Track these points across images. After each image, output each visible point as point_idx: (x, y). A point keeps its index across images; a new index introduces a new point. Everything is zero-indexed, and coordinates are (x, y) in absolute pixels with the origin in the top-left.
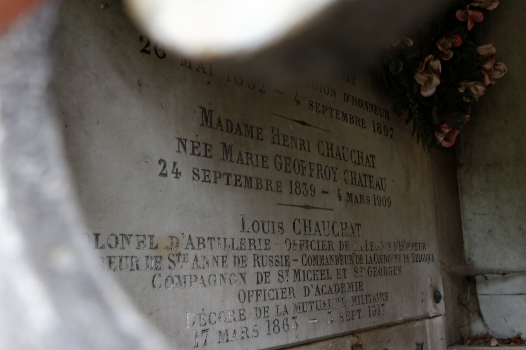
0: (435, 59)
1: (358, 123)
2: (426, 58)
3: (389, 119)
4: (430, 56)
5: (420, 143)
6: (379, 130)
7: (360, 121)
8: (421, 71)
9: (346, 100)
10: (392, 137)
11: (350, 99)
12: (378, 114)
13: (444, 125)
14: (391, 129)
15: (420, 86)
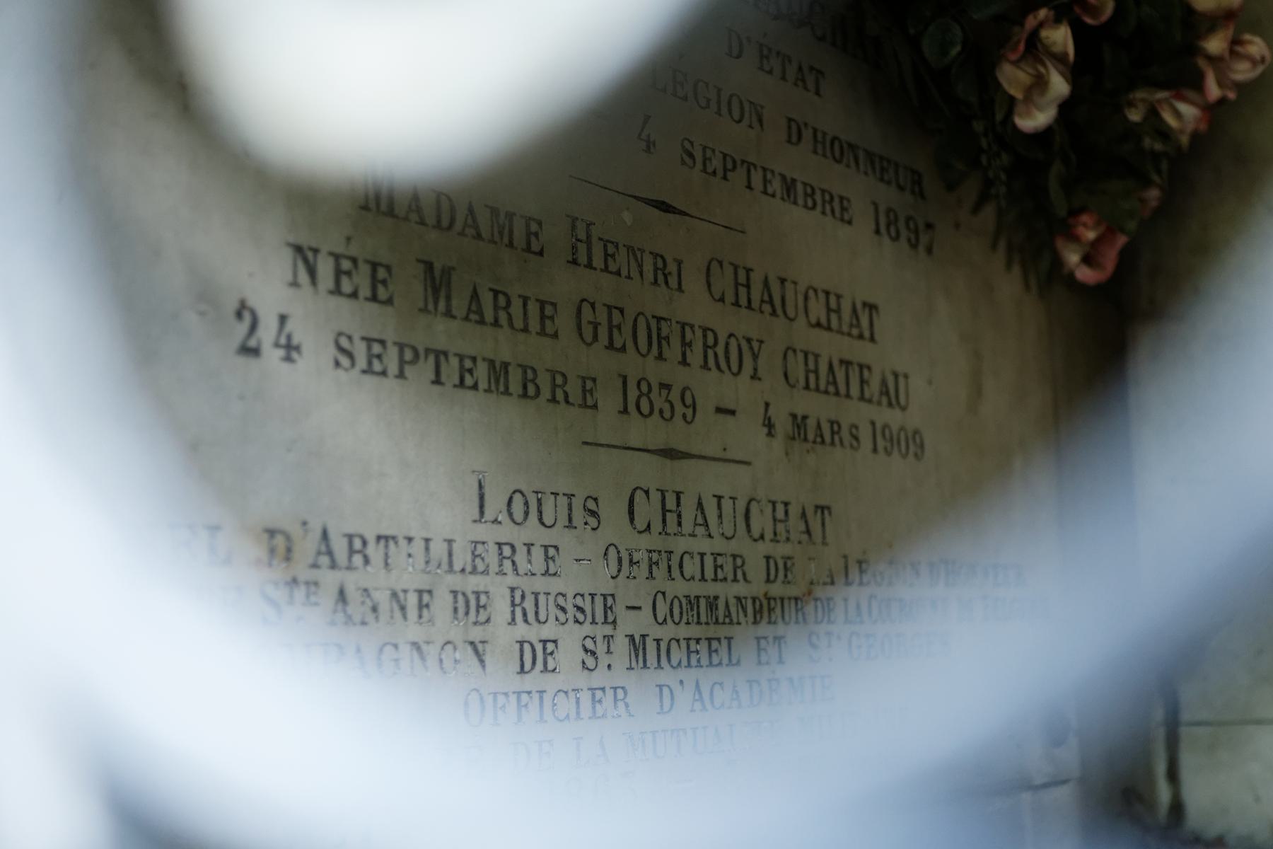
0: (1057, 21)
3: (922, 196)
5: (1016, 270)
8: (1014, 57)
9: (794, 139)
10: (929, 250)
11: (808, 134)
13: (1085, 218)
15: (1012, 100)
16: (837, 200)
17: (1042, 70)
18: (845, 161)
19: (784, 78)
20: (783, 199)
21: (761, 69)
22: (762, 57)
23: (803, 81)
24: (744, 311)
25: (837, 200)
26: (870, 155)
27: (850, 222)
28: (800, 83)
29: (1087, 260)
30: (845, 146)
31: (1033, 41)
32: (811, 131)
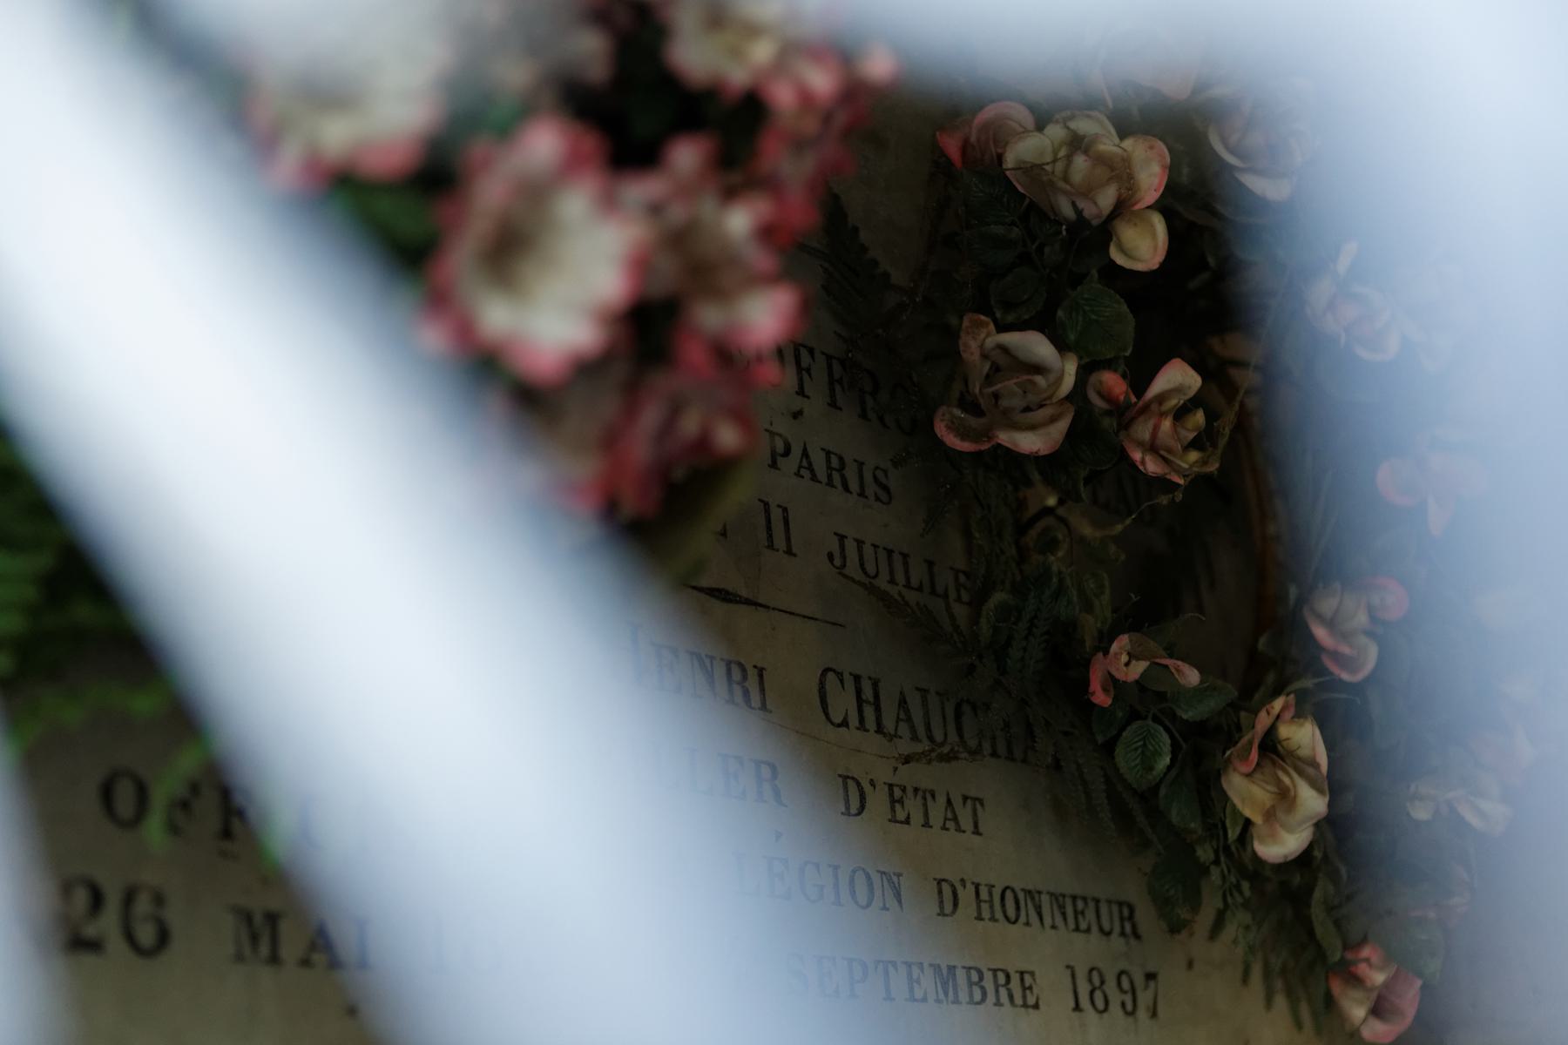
0: (1299, 715)
1: (1003, 992)
2: (1263, 714)
3: (1137, 936)
4: (1278, 704)
5: (1280, 1001)
6: (1098, 995)
7: (1015, 984)
8: (1245, 769)
9: (948, 907)
10: (1154, 1014)
11: (967, 895)
12: (1088, 930)
13: (1366, 952)
14: (1151, 976)
15: (1248, 823)
16: (1015, 979)
17: (1286, 780)
18: (1023, 919)
19: (926, 825)
20: (938, 1001)
21: (894, 820)
22: (893, 801)
23: (955, 819)
24: (983, 882)
25: (1015, 979)
26: (1057, 898)
27: (1036, 1006)
28: (950, 824)
29: (1377, 1011)
30: (1021, 896)
31: (1271, 747)
32: (971, 889)
